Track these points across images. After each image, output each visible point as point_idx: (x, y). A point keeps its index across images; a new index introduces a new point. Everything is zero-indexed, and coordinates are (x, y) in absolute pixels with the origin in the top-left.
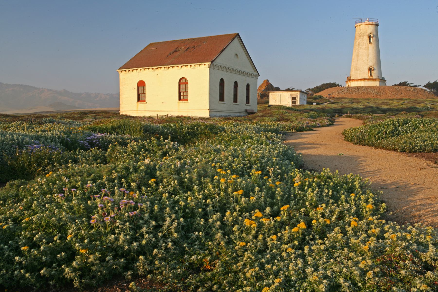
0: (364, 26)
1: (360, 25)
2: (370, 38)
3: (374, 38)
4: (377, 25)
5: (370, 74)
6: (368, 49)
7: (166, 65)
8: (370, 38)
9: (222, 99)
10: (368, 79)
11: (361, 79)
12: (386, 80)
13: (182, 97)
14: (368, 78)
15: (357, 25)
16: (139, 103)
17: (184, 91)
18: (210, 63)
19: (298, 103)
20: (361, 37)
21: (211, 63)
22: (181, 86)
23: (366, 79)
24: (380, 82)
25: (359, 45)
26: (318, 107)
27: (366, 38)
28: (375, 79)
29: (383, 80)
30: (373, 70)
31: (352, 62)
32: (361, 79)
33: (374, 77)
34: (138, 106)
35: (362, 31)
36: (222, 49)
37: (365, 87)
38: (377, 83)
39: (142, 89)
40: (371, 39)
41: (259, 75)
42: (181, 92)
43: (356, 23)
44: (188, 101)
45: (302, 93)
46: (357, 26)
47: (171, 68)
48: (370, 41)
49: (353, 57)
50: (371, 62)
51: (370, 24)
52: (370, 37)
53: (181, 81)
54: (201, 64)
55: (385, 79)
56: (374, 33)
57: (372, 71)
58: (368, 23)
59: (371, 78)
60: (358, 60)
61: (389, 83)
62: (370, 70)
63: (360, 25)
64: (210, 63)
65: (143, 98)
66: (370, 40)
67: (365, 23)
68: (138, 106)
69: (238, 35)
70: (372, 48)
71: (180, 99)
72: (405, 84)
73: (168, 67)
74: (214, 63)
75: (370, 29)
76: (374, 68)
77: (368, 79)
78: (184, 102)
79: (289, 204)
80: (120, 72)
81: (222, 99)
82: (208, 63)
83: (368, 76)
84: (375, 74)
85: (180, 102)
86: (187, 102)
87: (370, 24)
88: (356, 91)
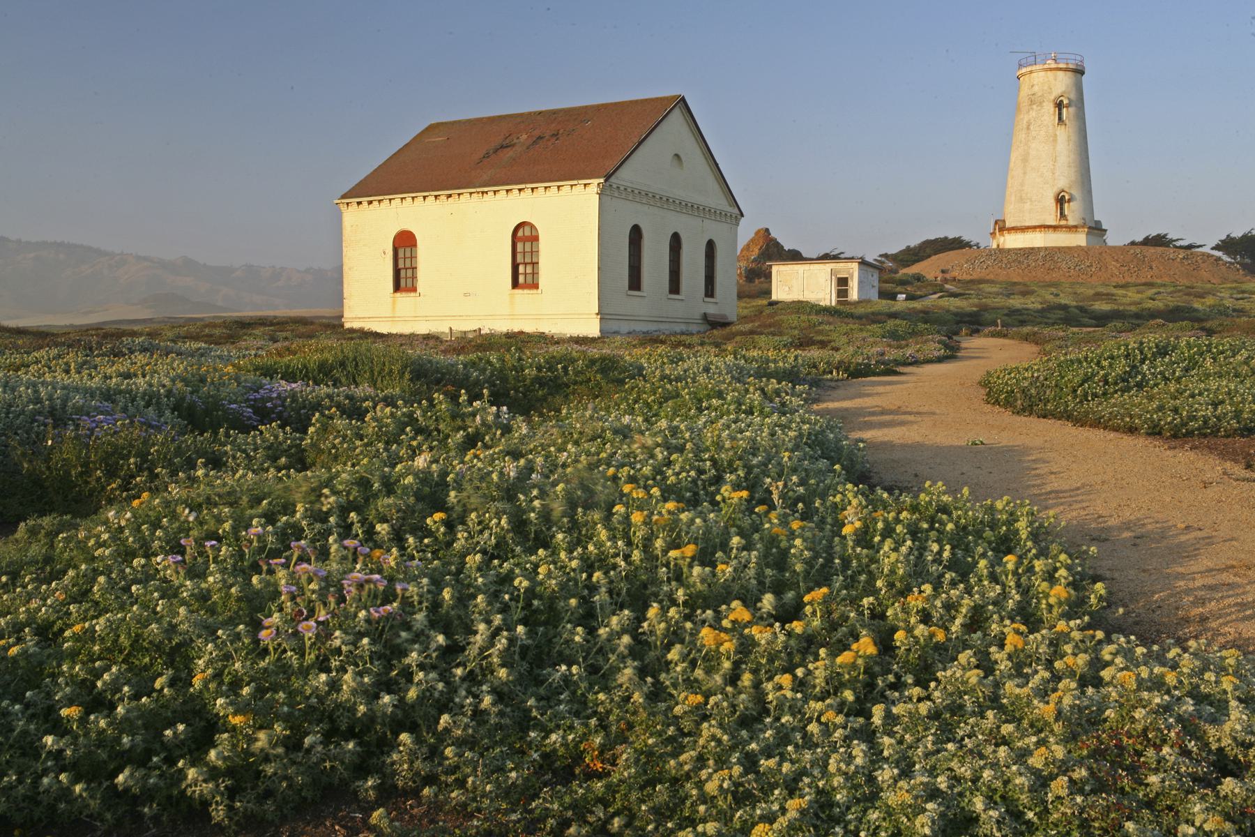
0: (1042, 74)
1: (1031, 72)
2: (1060, 110)
3: (1072, 110)
4: (1079, 72)
5: (1061, 213)
6: (1055, 140)
7: (474, 187)
8: (1060, 110)
9: (635, 282)
10: (1055, 228)
11: (1034, 228)
12: (1105, 231)
13: (521, 279)
14: (1053, 223)
15: (1024, 70)
16: (398, 295)
17: (528, 260)
18: (602, 180)
19: (854, 295)
20: (1034, 107)
21: (606, 181)
22: (520, 247)
23: (1049, 227)
24: (1088, 234)
25: (1028, 128)
26: (911, 306)
27: (1050, 108)
28: (1076, 227)
29: (1096, 230)
30: (1069, 201)
31: (1009, 179)
32: (1034, 228)
33: (1071, 222)
34: (394, 303)
35: (1036, 89)
36: (636, 140)
37: (1046, 248)
38: (1079, 239)
39: (408, 255)
40: (1064, 110)
41: (742, 215)
42: (518, 265)
43: (1020, 66)
44: (539, 291)
45: (865, 268)
46: (1023, 75)
47: (491, 194)
48: (1060, 119)
49: (1012, 165)
50: (1064, 178)
51: (1060, 69)
52: (1059, 106)
53: (520, 234)
54: (575, 182)
55: (1104, 227)
56: (1073, 96)
57: (1066, 205)
58: (1054, 66)
59: (1063, 223)
60: (1025, 173)
61: (1116, 238)
62: (1060, 201)
63: (1031, 72)
64: (602, 180)
65: (409, 281)
66: (1060, 114)
67: (1046, 66)
68: (394, 303)
69: (683, 100)
70: (1064, 138)
71: (515, 284)
72: (1159, 241)
73: (483, 193)
74: (613, 180)
75: (1061, 84)
76: (1071, 195)
77: (1055, 228)
78: (526, 291)
79: (829, 586)
80: (343, 208)
81: (635, 282)
82: (595, 182)
83: (1053, 217)
84: (1074, 212)
85: (517, 291)
86: (534, 291)
87: (1060, 69)
88: (1019, 262)
